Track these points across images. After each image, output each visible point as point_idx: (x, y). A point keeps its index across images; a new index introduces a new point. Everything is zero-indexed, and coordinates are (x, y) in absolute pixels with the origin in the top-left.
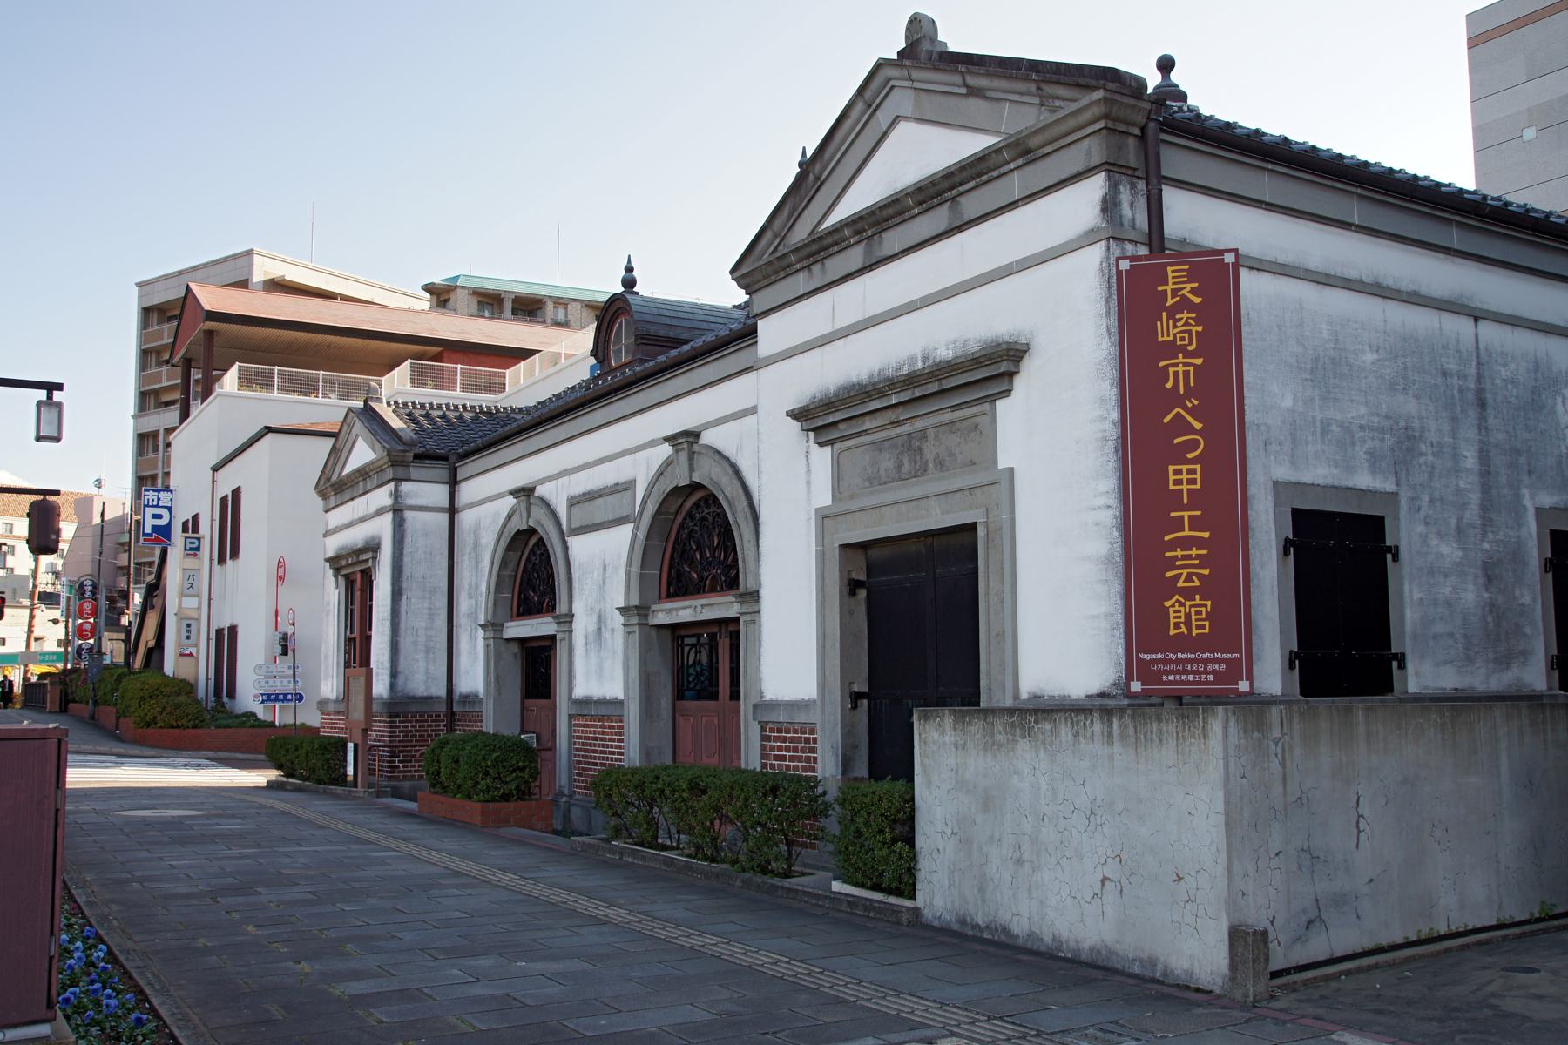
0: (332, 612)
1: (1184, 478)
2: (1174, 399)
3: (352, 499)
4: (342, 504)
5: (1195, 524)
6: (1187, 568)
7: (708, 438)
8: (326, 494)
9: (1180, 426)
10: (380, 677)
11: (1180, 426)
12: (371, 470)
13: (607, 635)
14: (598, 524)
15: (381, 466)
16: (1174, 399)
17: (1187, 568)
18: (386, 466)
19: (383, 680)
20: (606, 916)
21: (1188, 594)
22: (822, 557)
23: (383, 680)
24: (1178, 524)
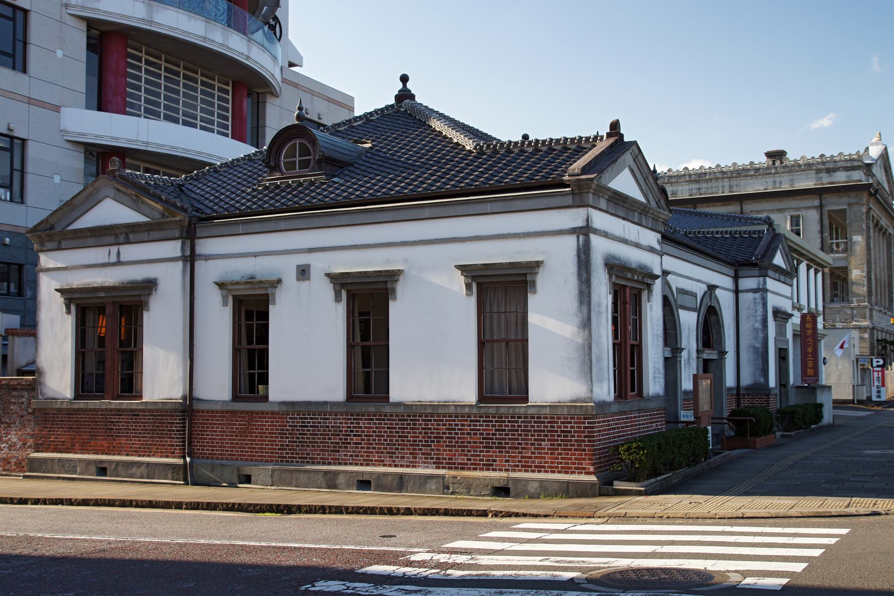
0: (604, 316)
1: (810, 350)
2: (808, 337)
3: (624, 219)
4: (611, 214)
5: (811, 357)
6: (810, 365)
7: (670, 278)
8: (600, 191)
9: (809, 341)
10: (657, 380)
11: (809, 341)
12: (652, 214)
13: (691, 361)
14: (685, 307)
15: (659, 217)
16: (808, 337)
17: (810, 365)
18: (661, 220)
19: (659, 382)
20: (367, 591)
21: (810, 368)
22: (775, 349)
23: (659, 382)
24: (809, 357)
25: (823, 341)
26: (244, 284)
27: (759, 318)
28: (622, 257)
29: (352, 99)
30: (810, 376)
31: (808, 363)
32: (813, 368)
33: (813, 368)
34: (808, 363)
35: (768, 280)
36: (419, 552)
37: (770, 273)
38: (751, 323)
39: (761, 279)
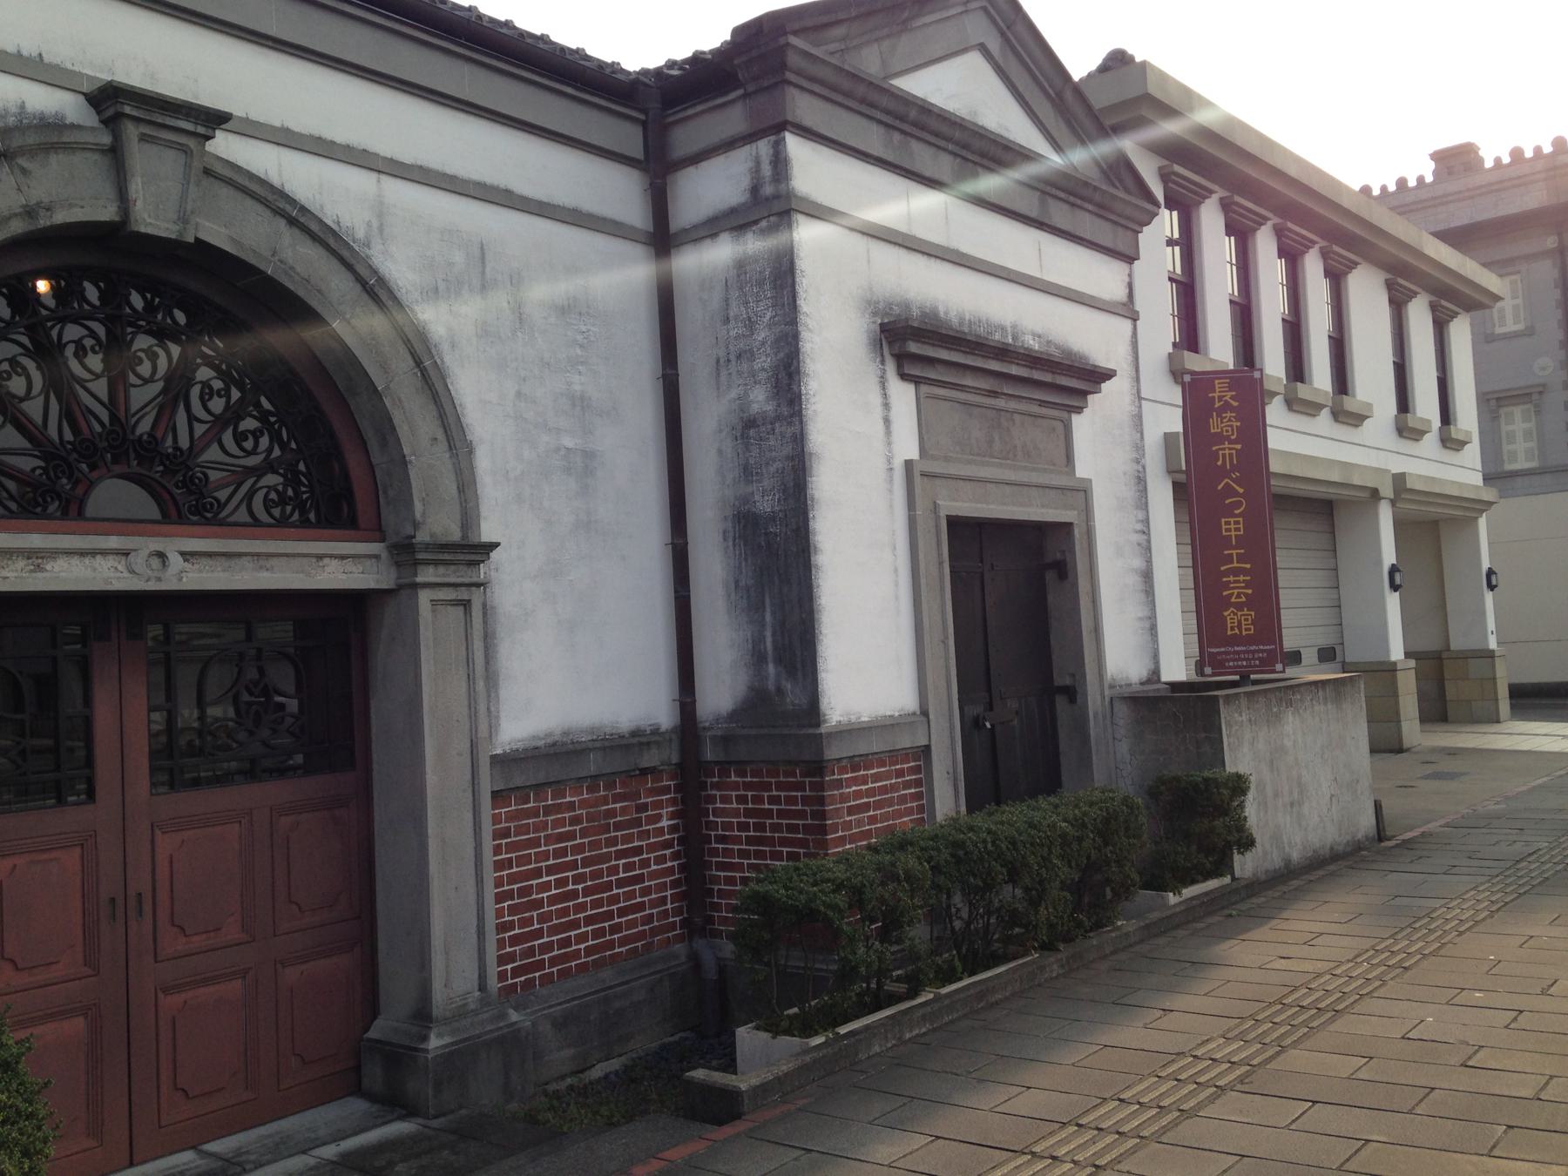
2: (1223, 473)
5: (1241, 559)
6: (1238, 589)
9: (1229, 491)
11: (1229, 491)
16: (1223, 473)
17: (1238, 589)
21: (1239, 606)
24: (1229, 559)
25: (1482, 522)
26: (897, 576)
27: (764, 361)
28: (915, 312)
29: (669, 60)
30: (1236, 640)
31: (1227, 586)
32: (1250, 603)
33: (1250, 603)
34: (1227, 586)
35: (795, 146)
36: (232, 687)
37: (804, 107)
38: (733, 394)
39: (763, 147)
